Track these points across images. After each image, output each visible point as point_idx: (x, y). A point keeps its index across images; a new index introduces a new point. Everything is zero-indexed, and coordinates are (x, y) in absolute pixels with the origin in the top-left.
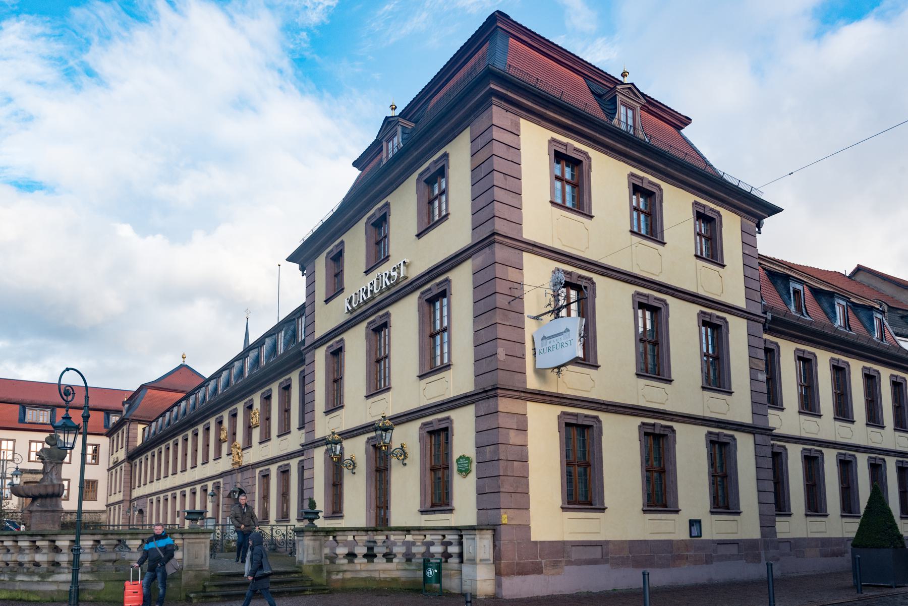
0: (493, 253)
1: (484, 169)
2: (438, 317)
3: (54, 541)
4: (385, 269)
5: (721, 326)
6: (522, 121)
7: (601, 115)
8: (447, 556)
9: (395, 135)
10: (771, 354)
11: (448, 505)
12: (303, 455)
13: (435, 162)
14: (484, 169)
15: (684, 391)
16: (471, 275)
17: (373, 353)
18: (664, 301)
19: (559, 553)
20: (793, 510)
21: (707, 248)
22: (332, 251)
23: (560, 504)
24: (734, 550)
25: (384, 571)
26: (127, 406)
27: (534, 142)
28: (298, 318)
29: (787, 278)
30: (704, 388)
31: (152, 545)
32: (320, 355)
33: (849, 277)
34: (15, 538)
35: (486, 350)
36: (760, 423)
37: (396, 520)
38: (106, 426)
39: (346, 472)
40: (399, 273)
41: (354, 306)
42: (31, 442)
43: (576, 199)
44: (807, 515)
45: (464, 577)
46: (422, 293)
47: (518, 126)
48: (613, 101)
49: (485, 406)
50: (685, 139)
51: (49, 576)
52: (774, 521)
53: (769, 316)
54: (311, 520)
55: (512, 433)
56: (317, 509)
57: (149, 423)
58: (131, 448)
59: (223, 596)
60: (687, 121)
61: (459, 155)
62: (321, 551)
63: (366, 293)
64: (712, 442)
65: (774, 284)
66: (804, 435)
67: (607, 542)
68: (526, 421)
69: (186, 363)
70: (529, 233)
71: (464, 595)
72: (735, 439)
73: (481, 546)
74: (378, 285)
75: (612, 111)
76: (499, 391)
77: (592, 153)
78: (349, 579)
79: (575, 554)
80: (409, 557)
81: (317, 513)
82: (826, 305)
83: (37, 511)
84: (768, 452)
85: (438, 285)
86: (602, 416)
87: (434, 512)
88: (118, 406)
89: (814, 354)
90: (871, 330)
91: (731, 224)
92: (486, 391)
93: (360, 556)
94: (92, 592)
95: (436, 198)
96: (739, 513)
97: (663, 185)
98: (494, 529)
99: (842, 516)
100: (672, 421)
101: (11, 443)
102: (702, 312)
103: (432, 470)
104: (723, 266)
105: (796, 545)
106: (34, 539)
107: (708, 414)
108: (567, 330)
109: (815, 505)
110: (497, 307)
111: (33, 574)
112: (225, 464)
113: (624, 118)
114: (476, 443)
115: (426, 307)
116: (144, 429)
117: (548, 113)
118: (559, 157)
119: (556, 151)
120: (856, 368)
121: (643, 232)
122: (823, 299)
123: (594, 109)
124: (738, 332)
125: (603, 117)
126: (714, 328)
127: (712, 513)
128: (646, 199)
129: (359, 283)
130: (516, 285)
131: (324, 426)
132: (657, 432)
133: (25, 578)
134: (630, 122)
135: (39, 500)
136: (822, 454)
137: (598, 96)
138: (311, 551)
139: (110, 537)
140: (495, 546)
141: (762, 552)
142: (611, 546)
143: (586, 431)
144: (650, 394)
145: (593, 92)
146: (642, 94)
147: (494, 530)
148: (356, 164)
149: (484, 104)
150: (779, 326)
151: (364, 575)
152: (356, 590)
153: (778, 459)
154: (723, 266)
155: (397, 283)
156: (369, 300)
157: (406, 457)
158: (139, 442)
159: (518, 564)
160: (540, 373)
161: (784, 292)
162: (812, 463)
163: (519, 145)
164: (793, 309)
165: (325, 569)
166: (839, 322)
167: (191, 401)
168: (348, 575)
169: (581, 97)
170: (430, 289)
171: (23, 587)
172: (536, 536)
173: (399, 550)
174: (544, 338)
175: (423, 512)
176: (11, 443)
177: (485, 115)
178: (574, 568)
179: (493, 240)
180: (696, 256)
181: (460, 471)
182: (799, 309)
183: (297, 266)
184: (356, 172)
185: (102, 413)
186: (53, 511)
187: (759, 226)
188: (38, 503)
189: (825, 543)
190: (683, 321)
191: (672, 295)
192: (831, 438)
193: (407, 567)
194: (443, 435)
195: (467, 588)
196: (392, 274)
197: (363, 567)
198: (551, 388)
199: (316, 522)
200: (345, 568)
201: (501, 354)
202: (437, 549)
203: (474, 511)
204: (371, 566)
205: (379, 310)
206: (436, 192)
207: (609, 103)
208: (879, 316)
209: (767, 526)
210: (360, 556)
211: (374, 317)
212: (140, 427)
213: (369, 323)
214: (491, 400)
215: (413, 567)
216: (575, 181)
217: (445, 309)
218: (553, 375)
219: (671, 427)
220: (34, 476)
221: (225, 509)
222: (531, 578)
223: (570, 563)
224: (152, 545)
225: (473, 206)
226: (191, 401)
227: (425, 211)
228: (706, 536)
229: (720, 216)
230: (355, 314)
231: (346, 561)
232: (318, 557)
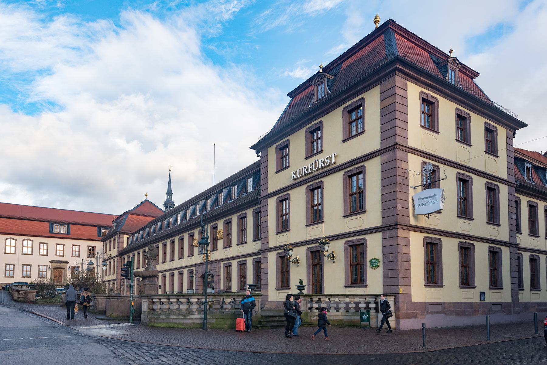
0: (395, 154)
2: (284, 208)
3: (152, 299)
4: (320, 158)
5: (468, 181)
7: (440, 76)
9: (323, 82)
10: (518, 203)
12: (260, 255)
13: (355, 102)
14: (389, 109)
15: (478, 226)
17: (310, 202)
18: (470, 177)
19: (424, 307)
21: (429, 122)
22: (280, 144)
23: (424, 283)
24: (499, 308)
25: (335, 316)
26: (115, 224)
27: (413, 93)
28: (248, 179)
29: (524, 161)
30: (487, 223)
31: (246, 301)
32: (272, 203)
33: (544, 155)
34: (168, 297)
35: (390, 204)
36: (512, 241)
37: (327, 290)
38: (99, 236)
39: (292, 265)
40: (331, 161)
41: (298, 176)
42: (57, 244)
43: (430, 123)
44: (531, 290)
47: (406, 85)
48: (446, 66)
49: (388, 234)
50: (476, 84)
51: (188, 316)
52: (518, 293)
53: (518, 183)
54: (301, 290)
55: (404, 247)
57: (133, 235)
58: (121, 249)
59: (271, 326)
60: (477, 74)
61: (372, 101)
62: (307, 305)
63: (307, 170)
67: (444, 303)
68: (409, 241)
69: (148, 199)
70: (412, 143)
72: (501, 250)
74: (316, 165)
75: (445, 74)
76: (399, 226)
77: (440, 98)
79: (431, 309)
80: (347, 310)
81: (304, 286)
82: (541, 175)
85: (357, 168)
86: (443, 238)
88: (109, 223)
91: (502, 133)
92: (390, 226)
94: (211, 324)
95: (354, 121)
96: (502, 289)
97: (471, 114)
98: (396, 296)
100: (473, 240)
102: (488, 182)
103: (351, 265)
105: (526, 306)
107: (489, 237)
108: (435, 195)
110: (393, 180)
111: (179, 314)
112: (198, 259)
113: (451, 76)
116: (128, 238)
117: (405, 69)
118: (424, 101)
119: (423, 98)
121: (427, 126)
122: (540, 172)
123: (433, 69)
124: (504, 191)
125: (446, 79)
126: (492, 191)
127: (490, 288)
129: (299, 162)
131: (274, 240)
132: (466, 246)
133: (175, 317)
134: (453, 78)
136: (522, 255)
137: (437, 64)
142: (446, 305)
143: (434, 246)
145: (434, 62)
146: (461, 64)
148: (289, 95)
149: (391, 74)
150: (521, 188)
153: (520, 259)
154: (470, 146)
155: (328, 166)
156: (309, 174)
159: (406, 313)
160: (415, 216)
161: (521, 169)
162: (534, 262)
164: (526, 178)
165: (309, 314)
167: (166, 222)
169: (426, 63)
171: (174, 321)
172: (414, 300)
173: (342, 306)
175: (346, 287)
179: (392, 146)
181: (372, 266)
183: (254, 151)
184: (289, 99)
186: (154, 284)
187: (514, 134)
190: (479, 186)
191: (474, 174)
192: (526, 246)
193: (346, 314)
194: (359, 249)
196: (326, 161)
202: (362, 306)
205: (316, 179)
207: (443, 68)
209: (515, 296)
210: (343, 309)
211: (313, 183)
212: (126, 237)
215: (350, 314)
216: (430, 113)
217: (287, 206)
218: (426, 218)
220: (59, 264)
221: (197, 284)
222: (412, 320)
223: (428, 313)
224: (246, 301)
225: (381, 128)
226: (166, 222)
227: (347, 128)
228: (487, 301)
229: (497, 129)
230: (297, 181)
232: (305, 309)
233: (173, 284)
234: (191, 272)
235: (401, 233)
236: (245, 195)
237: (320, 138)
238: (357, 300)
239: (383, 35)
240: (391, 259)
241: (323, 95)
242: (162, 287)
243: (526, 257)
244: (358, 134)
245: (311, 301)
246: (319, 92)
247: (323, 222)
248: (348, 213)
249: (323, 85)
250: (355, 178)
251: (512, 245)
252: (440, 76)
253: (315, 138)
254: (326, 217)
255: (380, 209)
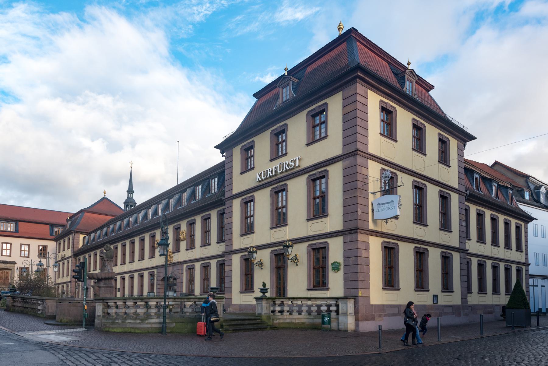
0: (356, 160)
1: (351, 116)
2: (249, 210)
3: (107, 303)
4: (285, 161)
6: (369, 91)
7: (398, 86)
8: (329, 311)
9: (288, 85)
10: (467, 211)
11: (325, 286)
12: (224, 257)
14: (351, 116)
16: (342, 170)
17: (275, 205)
19: (382, 309)
20: (473, 291)
21: (388, 130)
22: (245, 145)
24: (450, 310)
25: (298, 319)
26: (70, 222)
27: (374, 101)
29: (472, 171)
30: (440, 229)
33: (491, 167)
34: (124, 301)
36: (463, 247)
38: (51, 234)
39: (256, 268)
40: (295, 164)
41: (263, 178)
42: (3, 243)
44: (478, 293)
45: (340, 322)
46: (309, 176)
47: (367, 93)
48: (403, 78)
49: (349, 237)
50: (431, 97)
51: (146, 320)
53: (468, 193)
54: (264, 293)
55: (363, 251)
56: (267, 287)
57: (89, 234)
58: (76, 249)
59: (233, 330)
60: (432, 87)
61: (335, 106)
62: (270, 308)
63: (272, 172)
64: (417, 252)
65: (484, 183)
66: (479, 253)
67: (400, 305)
68: (369, 245)
69: (106, 197)
70: (372, 150)
71: (339, 330)
73: (350, 306)
75: (403, 84)
76: (359, 230)
78: (282, 323)
80: (309, 312)
81: (267, 289)
83: (103, 287)
84: (465, 261)
87: (317, 290)
88: (63, 222)
89: (484, 212)
90: (506, 199)
91: (453, 143)
92: (351, 230)
93: (286, 312)
95: (318, 125)
96: (453, 292)
98: (356, 299)
99: (493, 294)
101: (9, 245)
102: (441, 191)
103: (314, 268)
104: (450, 167)
105: (474, 308)
106: (195, 300)
107: (442, 243)
108: (392, 201)
109: (482, 289)
110: (354, 185)
111: (136, 319)
112: (159, 260)
114: (344, 256)
115: (311, 183)
116: (84, 238)
120: (501, 218)
121: (386, 134)
123: (392, 79)
124: (455, 199)
125: (403, 89)
126: (444, 199)
128: (418, 132)
129: (264, 165)
130: (366, 177)
134: (410, 90)
135: (103, 281)
137: (396, 74)
138: (265, 309)
139: (177, 300)
140: (355, 307)
141: (462, 311)
143: (392, 251)
144: (418, 232)
146: (418, 76)
147: (355, 299)
148: (255, 95)
149: (353, 81)
150: (471, 197)
151: (288, 321)
152: (296, 328)
153: (469, 264)
155: (293, 169)
156: (273, 176)
157: (298, 261)
158: (81, 245)
160: (375, 221)
161: (471, 179)
162: (481, 266)
163: (367, 103)
166: (494, 195)
168: (281, 321)
170: (315, 174)
172: (372, 303)
173: (305, 308)
174: (379, 204)
175: (309, 290)
176: (9, 245)
177: (352, 87)
178: (387, 317)
179: (353, 152)
180: (380, 133)
181: (333, 269)
182: (477, 188)
184: (255, 100)
185: (48, 226)
186: (111, 287)
187: (464, 146)
188: (102, 284)
189: (485, 307)
193: (308, 317)
195: (341, 327)
196: (290, 163)
197: (288, 317)
198: (379, 229)
199: (266, 294)
200: (280, 317)
201: (359, 213)
202: (324, 308)
203: (343, 289)
204: (291, 317)
206: (317, 122)
208: (511, 192)
209: (464, 299)
210: (305, 311)
211: (277, 185)
212: (81, 236)
213: (272, 189)
214: (353, 234)
215: (312, 317)
216: (389, 122)
217: (252, 207)
218: (384, 223)
219: (427, 249)
220: (6, 265)
222: (370, 322)
223: (385, 315)
227: (311, 132)
228: (439, 303)
231: (280, 314)
233: (132, 287)
234: (152, 275)
235: (361, 237)
236: (209, 195)
237: (284, 141)
238: (319, 303)
239: (345, 43)
240: (351, 263)
241: (288, 97)
242: (121, 290)
243: (474, 262)
244: (321, 139)
245: (274, 304)
246: (284, 95)
247: (287, 225)
248: (312, 217)
249: (288, 88)
250: (318, 182)
251: (462, 251)
252: (398, 86)
253: (280, 140)
254: (290, 220)
255: (342, 214)
